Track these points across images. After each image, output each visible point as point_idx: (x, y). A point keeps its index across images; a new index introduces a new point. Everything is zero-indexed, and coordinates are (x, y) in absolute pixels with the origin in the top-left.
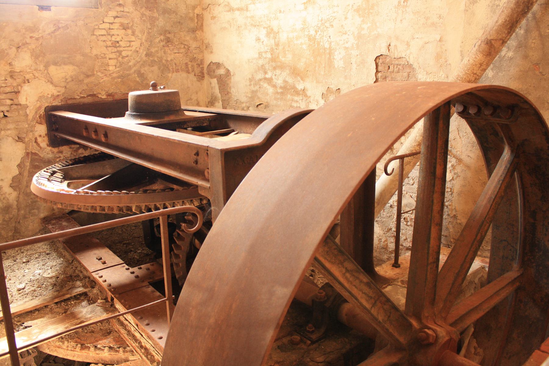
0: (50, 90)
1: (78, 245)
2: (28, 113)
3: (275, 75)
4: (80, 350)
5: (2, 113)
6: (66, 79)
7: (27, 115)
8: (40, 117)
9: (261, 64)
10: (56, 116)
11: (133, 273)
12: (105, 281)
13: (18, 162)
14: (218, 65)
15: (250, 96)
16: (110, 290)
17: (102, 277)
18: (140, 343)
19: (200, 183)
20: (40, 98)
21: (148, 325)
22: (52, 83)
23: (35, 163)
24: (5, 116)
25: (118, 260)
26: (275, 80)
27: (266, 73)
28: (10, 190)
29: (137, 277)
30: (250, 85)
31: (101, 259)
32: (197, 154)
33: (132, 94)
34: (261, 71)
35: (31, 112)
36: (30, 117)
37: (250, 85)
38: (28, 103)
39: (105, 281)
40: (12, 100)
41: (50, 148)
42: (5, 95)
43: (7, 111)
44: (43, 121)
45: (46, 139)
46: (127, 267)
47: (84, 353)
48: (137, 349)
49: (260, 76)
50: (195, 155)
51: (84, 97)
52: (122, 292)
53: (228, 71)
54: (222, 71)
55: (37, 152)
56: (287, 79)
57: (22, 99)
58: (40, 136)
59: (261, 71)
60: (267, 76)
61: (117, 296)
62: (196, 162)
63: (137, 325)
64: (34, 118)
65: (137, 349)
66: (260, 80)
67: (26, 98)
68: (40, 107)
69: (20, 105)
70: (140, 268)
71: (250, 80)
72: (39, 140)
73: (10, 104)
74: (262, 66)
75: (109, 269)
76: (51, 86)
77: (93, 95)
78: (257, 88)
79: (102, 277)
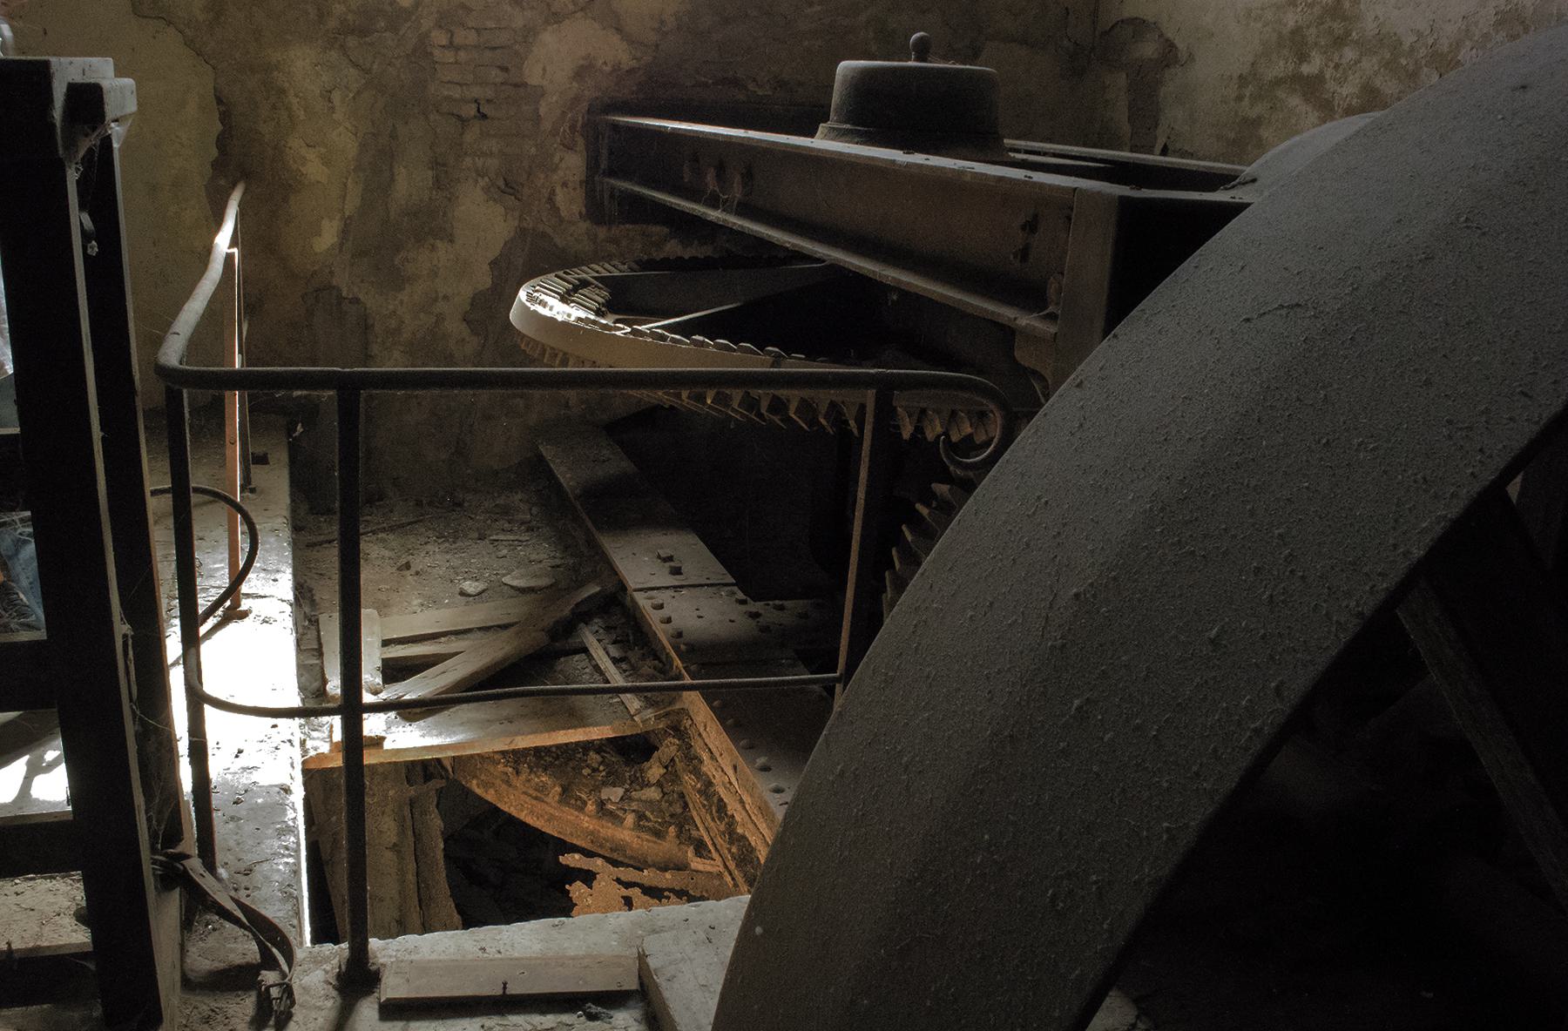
0: (613, 52)
1: (616, 507)
2: (542, 111)
3: (1337, 67)
4: (560, 802)
5: (474, 106)
6: (662, 22)
7: (537, 120)
8: (573, 128)
9: (1291, 24)
10: (616, 127)
11: (755, 616)
12: (669, 620)
13: (493, 254)
14: (1139, 26)
15: (1232, 135)
16: (676, 648)
17: (661, 607)
18: (731, 824)
19: (1025, 320)
20: (580, 73)
21: (765, 769)
22: (619, 30)
23: (538, 257)
24: (484, 116)
25: (718, 572)
26: (1331, 85)
27: (1303, 57)
28: (464, 330)
29: (765, 629)
30: (1240, 98)
31: (670, 559)
32: (1031, 226)
33: (847, 67)
34: (1285, 52)
35: (548, 108)
36: (547, 125)
37: (1240, 98)
38: (545, 83)
39: (669, 620)
40: (505, 69)
41: (584, 226)
42: (488, 54)
43: (488, 101)
44: (581, 142)
45: (579, 195)
46: (741, 595)
47: (569, 814)
48: (719, 841)
49: (1280, 67)
50: (1023, 228)
51: (706, 85)
52: (707, 657)
53: (1171, 46)
54: (1148, 49)
55: (549, 231)
56: (1378, 82)
57: (533, 75)
58: (565, 185)
59: (1285, 52)
60: (1306, 69)
61: (693, 668)
62: (1024, 254)
63: (735, 768)
64: (554, 133)
65: (719, 841)
66: (1278, 82)
67: (544, 69)
68: (576, 99)
69: (525, 85)
70: (781, 608)
71: (1243, 80)
72: (560, 197)
73: (498, 80)
74: (1297, 31)
75: (675, 584)
76: (615, 39)
77: (735, 83)
78: (1260, 109)
79: (661, 607)
